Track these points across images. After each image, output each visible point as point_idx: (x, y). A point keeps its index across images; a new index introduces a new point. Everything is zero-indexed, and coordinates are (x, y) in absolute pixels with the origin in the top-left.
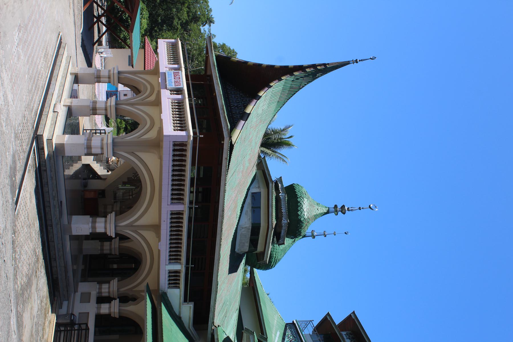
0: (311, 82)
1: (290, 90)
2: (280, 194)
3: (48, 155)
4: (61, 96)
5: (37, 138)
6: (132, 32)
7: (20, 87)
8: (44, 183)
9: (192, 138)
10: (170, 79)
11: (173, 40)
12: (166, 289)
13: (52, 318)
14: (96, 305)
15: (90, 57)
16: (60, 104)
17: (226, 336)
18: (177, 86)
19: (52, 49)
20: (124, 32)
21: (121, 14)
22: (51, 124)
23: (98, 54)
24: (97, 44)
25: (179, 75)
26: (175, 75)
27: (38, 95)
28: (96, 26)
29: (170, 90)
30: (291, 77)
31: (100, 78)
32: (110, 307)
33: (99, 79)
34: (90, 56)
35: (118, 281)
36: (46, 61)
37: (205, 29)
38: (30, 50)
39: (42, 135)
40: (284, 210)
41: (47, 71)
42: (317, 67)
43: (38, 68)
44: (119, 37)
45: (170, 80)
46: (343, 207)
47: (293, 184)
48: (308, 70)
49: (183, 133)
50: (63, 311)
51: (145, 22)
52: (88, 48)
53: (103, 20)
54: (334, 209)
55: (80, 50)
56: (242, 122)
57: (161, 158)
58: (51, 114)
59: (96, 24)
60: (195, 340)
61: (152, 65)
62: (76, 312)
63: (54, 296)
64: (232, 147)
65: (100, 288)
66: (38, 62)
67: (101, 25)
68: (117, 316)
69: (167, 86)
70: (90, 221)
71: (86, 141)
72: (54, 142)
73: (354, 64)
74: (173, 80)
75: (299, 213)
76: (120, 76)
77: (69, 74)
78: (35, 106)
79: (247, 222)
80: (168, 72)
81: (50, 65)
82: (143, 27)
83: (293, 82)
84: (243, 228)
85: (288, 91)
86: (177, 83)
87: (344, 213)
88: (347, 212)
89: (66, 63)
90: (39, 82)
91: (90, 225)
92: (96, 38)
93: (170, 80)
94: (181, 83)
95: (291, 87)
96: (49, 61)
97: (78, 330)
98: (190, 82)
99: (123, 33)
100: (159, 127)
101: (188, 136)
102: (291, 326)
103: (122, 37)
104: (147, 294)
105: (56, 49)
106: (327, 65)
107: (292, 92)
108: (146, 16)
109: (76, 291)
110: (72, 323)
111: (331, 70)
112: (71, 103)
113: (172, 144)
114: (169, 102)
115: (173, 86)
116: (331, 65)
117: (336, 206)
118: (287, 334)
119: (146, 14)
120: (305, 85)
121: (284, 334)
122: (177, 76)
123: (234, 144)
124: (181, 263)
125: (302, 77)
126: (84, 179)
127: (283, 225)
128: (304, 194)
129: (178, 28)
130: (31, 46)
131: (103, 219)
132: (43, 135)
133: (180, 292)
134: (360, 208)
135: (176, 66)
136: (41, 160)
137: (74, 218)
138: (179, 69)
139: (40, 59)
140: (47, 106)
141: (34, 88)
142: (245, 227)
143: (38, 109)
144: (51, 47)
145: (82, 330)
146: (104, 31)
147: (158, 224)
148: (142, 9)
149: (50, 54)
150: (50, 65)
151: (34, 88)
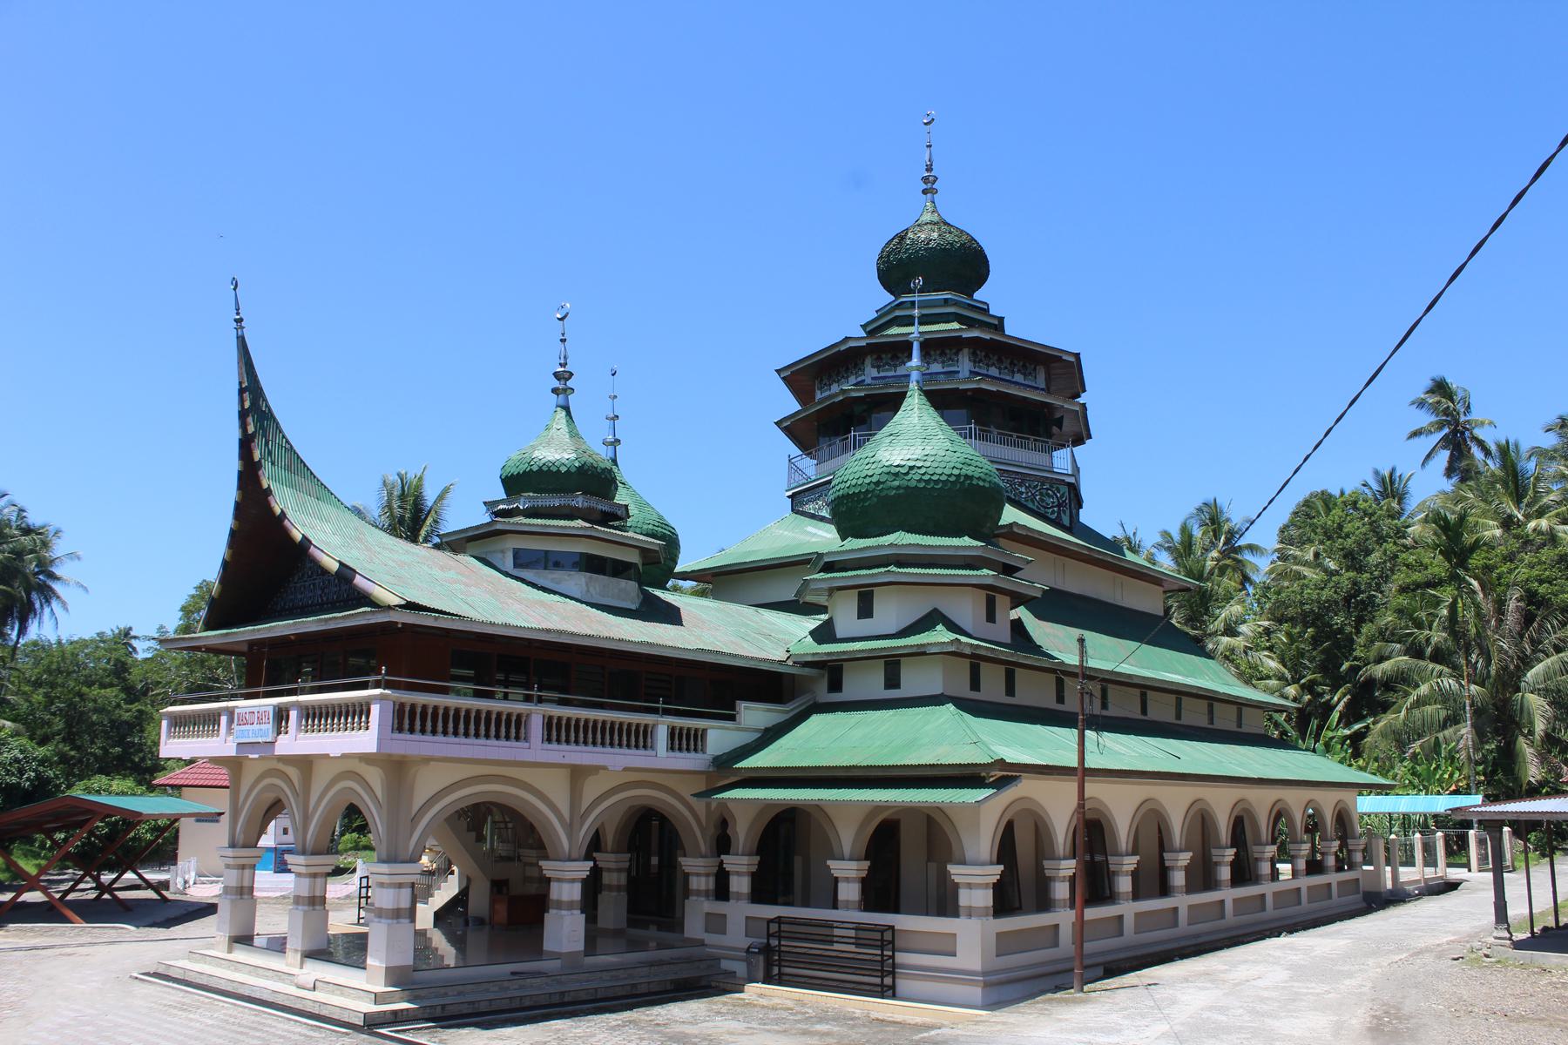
0: (278, 423)
2: (521, 508)
3: (409, 1001)
6: (140, 814)
9: (387, 691)
11: (164, 723)
13: (754, 990)
16: (298, 975)
21: (97, 837)
22: (342, 994)
23: (187, 891)
24: (164, 893)
26: (244, 722)
27: (274, 1024)
28: (121, 895)
32: (847, 880)
33: (246, 891)
34: (191, 909)
35: (685, 856)
39: (365, 1014)
41: (221, 1004)
43: (212, 1026)
48: (251, 429)
49: (375, 709)
50: (740, 968)
52: (172, 913)
53: (107, 877)
54: (560, 396)
55: (177, 931)
56: (358, 580)
57: (427, 760)
58: (319, 996)
60: (811, 702)
62: (744, 942)
63: (710, 987)
64: (411, 606)
65: (698, 893)
68: (867, 864)
71: (383, 921)
72: (381, 988)
74: (256, 727)
75: (563, 469)
76: (241, 842)
79: (577, 581)
81: (207, 997)
87: (571, 374)
88: (568, 368)
89: (205, 963)
91: (564, 912)
94: (263, 709)
97: (780, 938)
98: (262, 689)
101: (381, 698)
102: (797, 501)
104: (715, 797)
105: (171, 984)
106: (244, 386)
107: (297, 467)
109: (702, 943)
110: (767, 950)
114: (306, 738)
115: (269, 727)
118: (812, 512)
119: (99, 781)
120: (284, 437)
121: (813, 516)
124: (654, 725)
125: (267, 444)
129: (139, 711)
131: (554, 886)
133: (713, 728)
134: (561, 340)
135: (224, 719)
136: (420, 1016)
138: (231, 713)
139: (191, 1020)
141: (258, 1034)
143: (305, 1024)
144: (165, 995)
145: (780, 931)
146: (135, 876)
148: (88, 790)
150: (207, 997)
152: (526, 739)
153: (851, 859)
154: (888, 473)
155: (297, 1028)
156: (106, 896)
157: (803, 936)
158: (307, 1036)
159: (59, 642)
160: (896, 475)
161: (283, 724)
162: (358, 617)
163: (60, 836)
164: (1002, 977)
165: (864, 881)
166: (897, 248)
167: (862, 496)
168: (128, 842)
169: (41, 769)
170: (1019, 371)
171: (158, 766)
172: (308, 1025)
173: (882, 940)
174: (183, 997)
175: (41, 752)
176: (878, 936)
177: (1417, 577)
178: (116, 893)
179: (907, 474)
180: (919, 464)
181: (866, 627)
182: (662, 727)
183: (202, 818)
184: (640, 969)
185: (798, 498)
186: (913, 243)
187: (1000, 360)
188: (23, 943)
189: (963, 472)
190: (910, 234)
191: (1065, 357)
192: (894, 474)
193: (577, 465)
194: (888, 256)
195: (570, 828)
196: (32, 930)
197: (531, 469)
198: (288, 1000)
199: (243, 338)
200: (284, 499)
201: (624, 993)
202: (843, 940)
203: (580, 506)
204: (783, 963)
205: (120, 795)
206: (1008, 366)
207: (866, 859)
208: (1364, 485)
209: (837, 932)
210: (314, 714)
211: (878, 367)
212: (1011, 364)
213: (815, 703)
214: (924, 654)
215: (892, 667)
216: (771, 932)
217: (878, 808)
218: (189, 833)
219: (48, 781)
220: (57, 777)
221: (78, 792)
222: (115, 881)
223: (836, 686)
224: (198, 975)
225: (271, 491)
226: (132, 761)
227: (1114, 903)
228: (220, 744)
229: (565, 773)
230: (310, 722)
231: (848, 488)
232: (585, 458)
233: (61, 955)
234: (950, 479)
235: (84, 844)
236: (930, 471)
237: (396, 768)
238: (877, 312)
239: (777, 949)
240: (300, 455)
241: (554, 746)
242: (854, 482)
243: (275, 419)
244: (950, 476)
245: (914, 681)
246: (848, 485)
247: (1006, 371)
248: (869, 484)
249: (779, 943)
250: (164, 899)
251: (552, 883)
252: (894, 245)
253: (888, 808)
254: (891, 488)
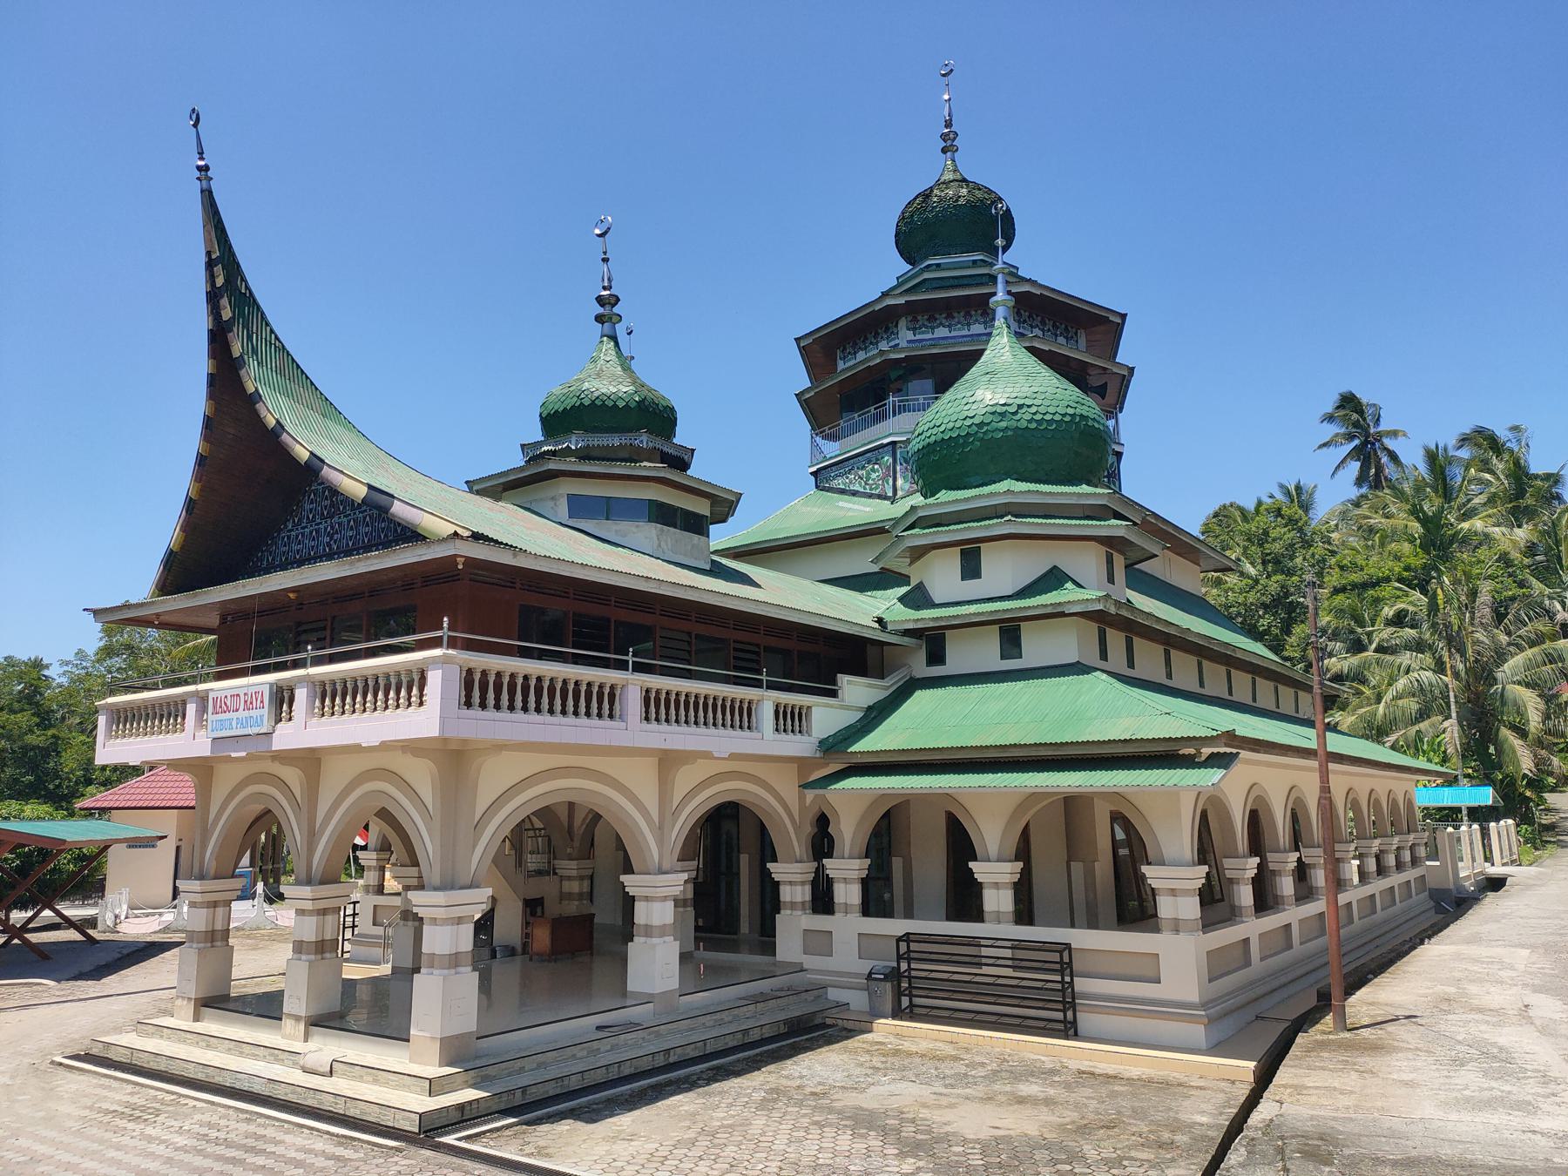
0: (263, 313)
1: (287, 377)
2: (573, 448)
3: (475, 1086)
4: (275, 1053)
8: (558, 1091)
9: (450, 651)
10: (237, 724)
11: (102, 720)
12: (811, 739)
14: (838, 916)
15: (131, 950)
16: (305, 1054)
17: (899, 603)
18: (262, 702)
20: (59, 863)
22: (376, 1081)
23: (119, 928)
24: (90, 932)
25: (226, 697)
27: (280, 1136)
28: (34, 938)
29: (276, 723)
30: (249, 365)
31: (213, 931)
32: (996, 885)
33: (219, 936)
34: (125, 952)
36: (157, 1113)
37: (56, 674)
40: (615, 441)
41: (192, 1103)
42: (218, 286)
43: (184, 1149)
44: (74, 874)
45: (242, 724)
46: (600, 300)
47: (540, 415)
48: (227, 314)
49: (434, 678)
50: (857, 1000)
52: (104, 958)
54: (606, 324)
55: (112, 983)
56: (398, 509)
57: (500, 747)
58: (339, 1085)
60: (908, 678)
61: (175, 778)
62: (865, 967)
64: (477, 537)
65: (793, 905)
66: (162, 1147)
67: (37, 923)
69: (264, 730)
70: (646, 942)
71: (436, 972)
72: (436, 1071)
73: (212, 179)
74: (242, 714)
75: (621, 404)
76: (212, 872)
77: (199, 1027)
78: (319, 1145)
80: (213, 731)
82: (47, 813)
83: (264, 364)
84: (659, 545)
85: (292, 383)
86: (251, 703)
87: (618, 300)
88: (613, 291)
89: (162, 1037)
90: (232, 1136)
91: (655, 940)
92: (72, 935)
93: (242, 724)
94: (253, 690)
95: (278, 371)
97: (909, 960)
98: (251, 664)
99: (63, 864)
100: (400, 752)
101: (445, 661)
102: (821, 478)
103: (75, 867)
104: (833, 787)
106: (214, 257)
107: (293, 373)
108: (13, 806)
110: (894, 975)
111: (230, 249)
112: (297, 1018)
113: (466, 712)
115: (264, 713)
116: (213, 247)
118: (842, 486)
120: (272, 331)
121: (842, 492)
122: (228, 704)
123: (472, 531)
124: (758, 701)
125: (250, 338)
126: (494, 956)
127: (651, 445)
128: (571, 389)
129: (54, 736)
132: (421, 1112)
133: (818, 705)
134: (603, 260)
135: (191, 709)
136: (495, 1108)
137: (631, 986)
138: (202, 699)
139: (150, 1139)
140: (314, 1098)
141: (260, 1161)
142: (658, 539)
143: (328, 1133)
144: (105, 1093)
145: (909, 951)
146: (52, 914)
147: (657, 759)
149: (128, 1098)
150: (168, 1092)
151: (260, 1161)
154: (993, 413)
155: (314, 1140)
158: (338, 1159)
160: (1003, 415)
161: (285, 707)
162: (406, 556)
166: (922, 207)
167: (961, 441)
168: (45, 875)
170: (1061, 334)
172: (332, 1134)
176: (1056, 957)
178: (28, 936)
179: (1015, 413)
180: (1028, 402)
181: (973, 588)
182: (767, 701)
183: (135, 843)
184: (745, 1009)
185: (824, 473)
187: (1043, 323)
189: (1078, 411)
190: (935, 191)
192: (1000, 414)
193: (637, 399)
194: (912, 216)
197: (581, 403)
199: (210, 192)
200: (276, 408)
201: (735, 1043)
202: (996, 962)
203: (645, 447)
204: (915, 992)
206: (1051, 328)
208: (1270, 497)
209: (985, 951)
211: (914, 329)
212: (965, 317)
213: (911, 678)
214: (1063, 615)
216: (901, 952)
217: (884, 796)
218: (117, 865)
222: (31, 920)
223: (936, 656)
225: (260, 396)
226: (46, 788)
228: (190, 741)
229: (652, 762)
231: (942, 432)
234: (1065, 419)
236: (1043, 410)
238: (898, 278)
239: (906, 974)
240: (291, 352)
241: (654, 726)
242: (951, 425)
243: (259, 307)
244: (1064, 415)
245: (1038, 647)
246: (942, 429)
247: (1049, 333)
248: (969, 426)
249: (909, 966)
250: (90, 939)
251: (636, 903)
252: (918, 204)
254: (997, 429)
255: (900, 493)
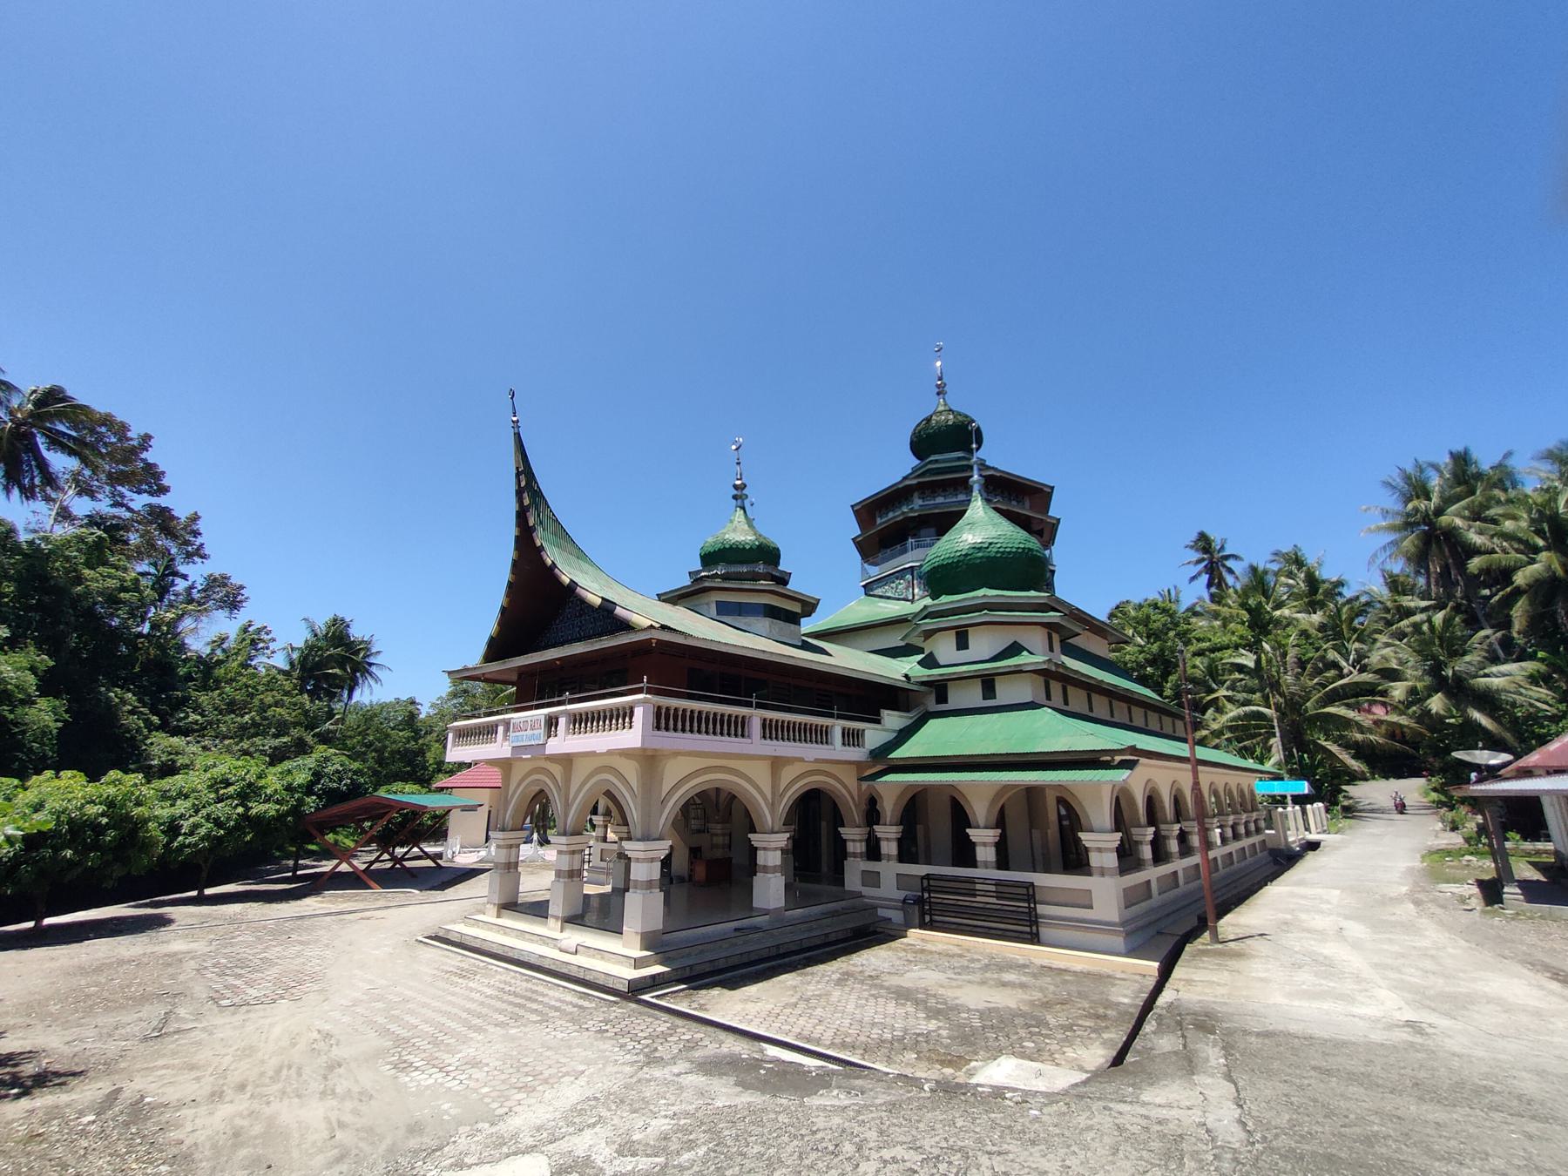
3: (662, 964)
4: (544, 940)
5: (634, 991)
6: (426, 807)
7: (540, 1050)
9: (648, 696)
11: (450, 736)
13: (915, 935)
19: (448, 957)
21: (392, 823)
23: (455, 859)
24: (439, 861)
26: (518, 729)
27: (546, 991)
28: (408, 864)
32: (985, 844)
33: (513, 865)
34: (459, 874)
35: (843, 826)
38: (453, 1025)
39: (629, 981)
41: (495, 968)
43: (490, 997)
48: (526, 502)
49: (639, 712)
50: (896, 916)
51: (409, 787)
52: (446, 878)
53: (399, 851)
55: (450, 892)
56: (618, 611)
57: (677, 754)
59: (404, 863)
62: (901, 895)
63: (875, 933)
64: (664, 627)
65: (855, 855)
68: (901, 828)
74: (529, 732)
75: (748, 547)
76: (639, 835)
79: (764, 623)
81: (482, 961)
87: (745, 486)
88: (744, 481)
91: (770, 875)
94: (535, 718)
96: (474, 965)
101: (644, 702)
102: (868, 589)
105: (450, 948)
107: (562, 535)
109: (860, 895)
110: (920, 901)
114: (572, 739)
115: (542, 731)
117: (735, 497)
119: (398, 786)
121: (881, 597)
125: (539, 515)
130: (443, 1020)
131: (760, 854)
135: (501, 729)
138: (507, 724)
139: (472, 990)
141: (535, 1006)
143: (574, 990)
148: (388, 792)
149: (459, 964)
150: (482, 961)
151: (535, 1006)
152: (749, 737)
153: (986, 828)
156: (398, 866)
157: (940, 889)
158: (581, 1007)
159: (371, 705)
160: (980, 549)
163: (367, 824)
164: (1140, 923)
165: (899, 841)
169: (355, 777)
171: (441, 767)
173: (1028, 895)
174: (461, 961)
175: (356, 765)
176: (1024, 891)
177: (1205, 645)
180: (996, 541)
181: (964, 655)
182: (837, 726)
183: (467, 809)
185: (869, 586)
186: (937, 422)
188: (334, 908)
191: (1045, 489)
195: (772, 806)
196: (342, 896)
198: (554, 964)
199: (519, 434)
200: (552, 555)
202: (986, 894)
205: (408, 794)
207: (901, 824)
209: (978, 887)
210: (587, 718)
215: (988, 684)
219: (360, 785)
220: (366, 783)
221: (382, 793)
222: (406, 853)
223: (942, 698)
224: (472, 939)
227: (1168, 862)
228: (498, 748)
230: (577, 726)
232: (762, 540)
233: (362, 919)
235: (384, 830)
237: (648, 759)
245: (1007, 692)
253: (1018, 785)
254: (977, 558)
255: (916, 598)
